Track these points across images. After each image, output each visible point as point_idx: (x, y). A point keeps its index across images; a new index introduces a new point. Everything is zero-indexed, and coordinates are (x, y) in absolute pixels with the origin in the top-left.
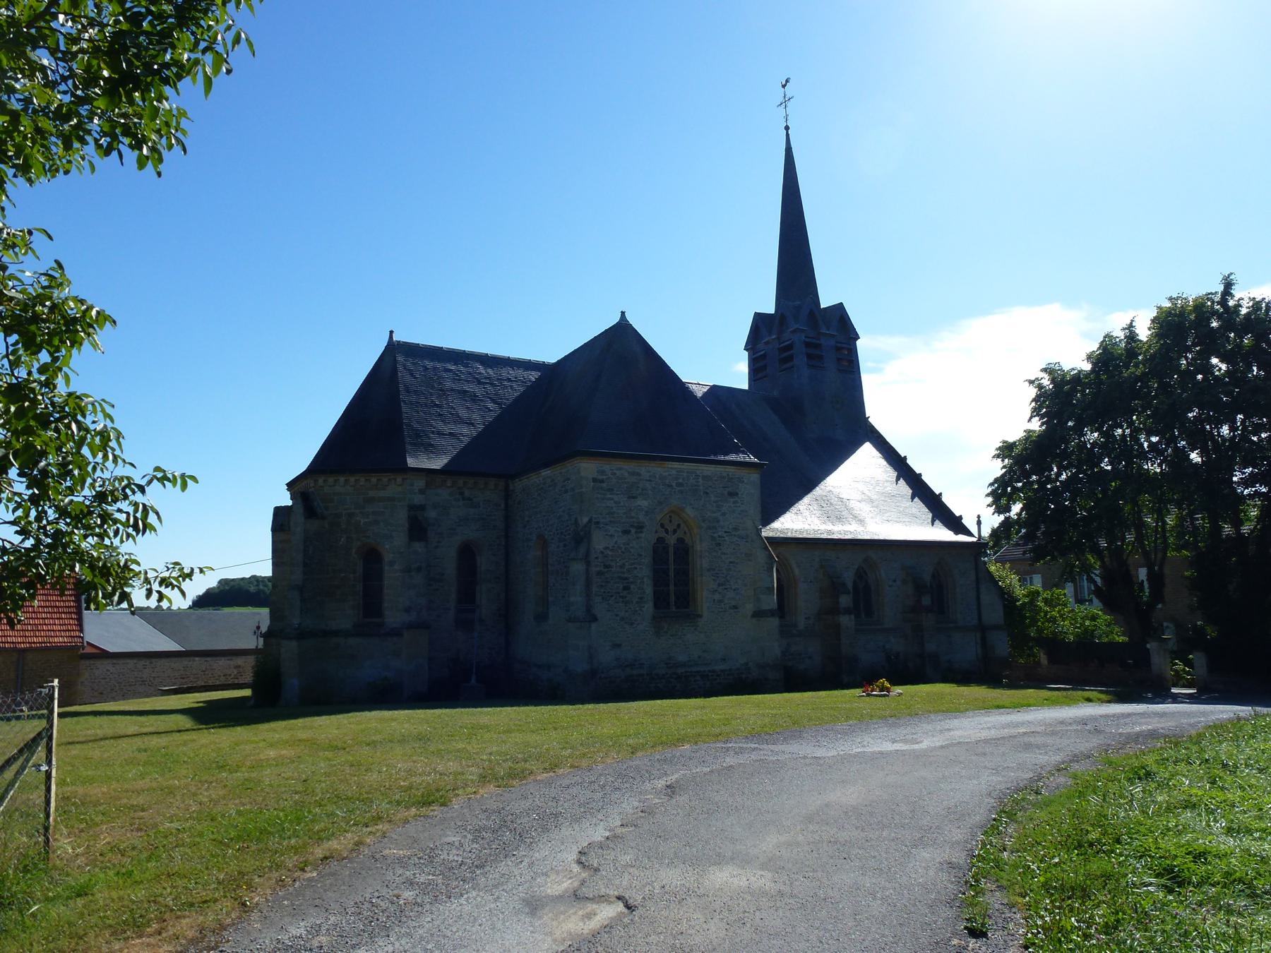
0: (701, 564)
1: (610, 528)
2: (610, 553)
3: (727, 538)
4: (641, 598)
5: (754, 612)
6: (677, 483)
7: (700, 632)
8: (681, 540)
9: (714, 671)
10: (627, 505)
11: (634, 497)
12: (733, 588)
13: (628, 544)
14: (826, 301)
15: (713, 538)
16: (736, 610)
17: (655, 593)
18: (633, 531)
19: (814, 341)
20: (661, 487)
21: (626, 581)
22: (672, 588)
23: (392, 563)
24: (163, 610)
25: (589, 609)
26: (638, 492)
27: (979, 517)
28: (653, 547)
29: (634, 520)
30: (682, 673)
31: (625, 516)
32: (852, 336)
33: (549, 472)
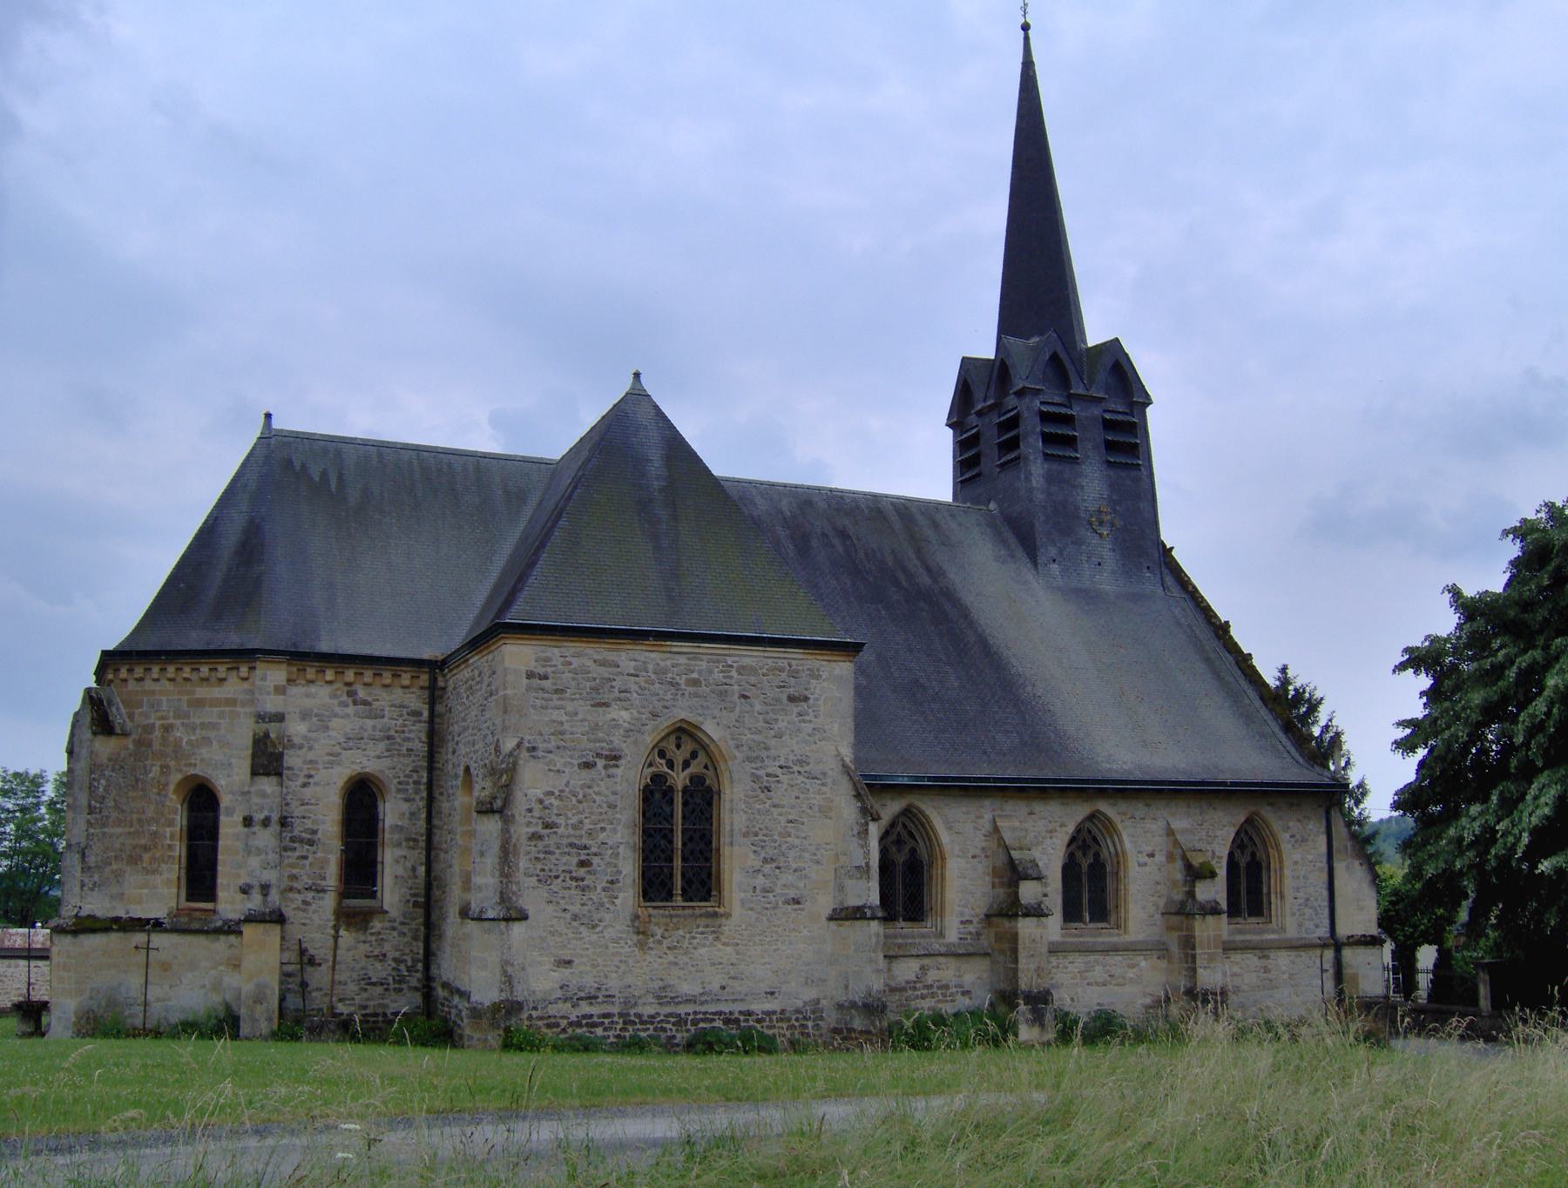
0: (732, 824)
1: (557, 759)
2: (556, 803)
4: (612, 882)
7: (724, 944)
8: (697, 780)
9: (749, 1013)
10: (589, 718)
11: (606, 705)
12: (794, 866)
13: (589, 787)
14: (1095, 334)
15: (756, 778)
16: (796, 906)
19: (1063, 411)
20: (657, 685)
22: (678, 862)
25: (504, 899)
26: (612, 696)
29: (604, 744)
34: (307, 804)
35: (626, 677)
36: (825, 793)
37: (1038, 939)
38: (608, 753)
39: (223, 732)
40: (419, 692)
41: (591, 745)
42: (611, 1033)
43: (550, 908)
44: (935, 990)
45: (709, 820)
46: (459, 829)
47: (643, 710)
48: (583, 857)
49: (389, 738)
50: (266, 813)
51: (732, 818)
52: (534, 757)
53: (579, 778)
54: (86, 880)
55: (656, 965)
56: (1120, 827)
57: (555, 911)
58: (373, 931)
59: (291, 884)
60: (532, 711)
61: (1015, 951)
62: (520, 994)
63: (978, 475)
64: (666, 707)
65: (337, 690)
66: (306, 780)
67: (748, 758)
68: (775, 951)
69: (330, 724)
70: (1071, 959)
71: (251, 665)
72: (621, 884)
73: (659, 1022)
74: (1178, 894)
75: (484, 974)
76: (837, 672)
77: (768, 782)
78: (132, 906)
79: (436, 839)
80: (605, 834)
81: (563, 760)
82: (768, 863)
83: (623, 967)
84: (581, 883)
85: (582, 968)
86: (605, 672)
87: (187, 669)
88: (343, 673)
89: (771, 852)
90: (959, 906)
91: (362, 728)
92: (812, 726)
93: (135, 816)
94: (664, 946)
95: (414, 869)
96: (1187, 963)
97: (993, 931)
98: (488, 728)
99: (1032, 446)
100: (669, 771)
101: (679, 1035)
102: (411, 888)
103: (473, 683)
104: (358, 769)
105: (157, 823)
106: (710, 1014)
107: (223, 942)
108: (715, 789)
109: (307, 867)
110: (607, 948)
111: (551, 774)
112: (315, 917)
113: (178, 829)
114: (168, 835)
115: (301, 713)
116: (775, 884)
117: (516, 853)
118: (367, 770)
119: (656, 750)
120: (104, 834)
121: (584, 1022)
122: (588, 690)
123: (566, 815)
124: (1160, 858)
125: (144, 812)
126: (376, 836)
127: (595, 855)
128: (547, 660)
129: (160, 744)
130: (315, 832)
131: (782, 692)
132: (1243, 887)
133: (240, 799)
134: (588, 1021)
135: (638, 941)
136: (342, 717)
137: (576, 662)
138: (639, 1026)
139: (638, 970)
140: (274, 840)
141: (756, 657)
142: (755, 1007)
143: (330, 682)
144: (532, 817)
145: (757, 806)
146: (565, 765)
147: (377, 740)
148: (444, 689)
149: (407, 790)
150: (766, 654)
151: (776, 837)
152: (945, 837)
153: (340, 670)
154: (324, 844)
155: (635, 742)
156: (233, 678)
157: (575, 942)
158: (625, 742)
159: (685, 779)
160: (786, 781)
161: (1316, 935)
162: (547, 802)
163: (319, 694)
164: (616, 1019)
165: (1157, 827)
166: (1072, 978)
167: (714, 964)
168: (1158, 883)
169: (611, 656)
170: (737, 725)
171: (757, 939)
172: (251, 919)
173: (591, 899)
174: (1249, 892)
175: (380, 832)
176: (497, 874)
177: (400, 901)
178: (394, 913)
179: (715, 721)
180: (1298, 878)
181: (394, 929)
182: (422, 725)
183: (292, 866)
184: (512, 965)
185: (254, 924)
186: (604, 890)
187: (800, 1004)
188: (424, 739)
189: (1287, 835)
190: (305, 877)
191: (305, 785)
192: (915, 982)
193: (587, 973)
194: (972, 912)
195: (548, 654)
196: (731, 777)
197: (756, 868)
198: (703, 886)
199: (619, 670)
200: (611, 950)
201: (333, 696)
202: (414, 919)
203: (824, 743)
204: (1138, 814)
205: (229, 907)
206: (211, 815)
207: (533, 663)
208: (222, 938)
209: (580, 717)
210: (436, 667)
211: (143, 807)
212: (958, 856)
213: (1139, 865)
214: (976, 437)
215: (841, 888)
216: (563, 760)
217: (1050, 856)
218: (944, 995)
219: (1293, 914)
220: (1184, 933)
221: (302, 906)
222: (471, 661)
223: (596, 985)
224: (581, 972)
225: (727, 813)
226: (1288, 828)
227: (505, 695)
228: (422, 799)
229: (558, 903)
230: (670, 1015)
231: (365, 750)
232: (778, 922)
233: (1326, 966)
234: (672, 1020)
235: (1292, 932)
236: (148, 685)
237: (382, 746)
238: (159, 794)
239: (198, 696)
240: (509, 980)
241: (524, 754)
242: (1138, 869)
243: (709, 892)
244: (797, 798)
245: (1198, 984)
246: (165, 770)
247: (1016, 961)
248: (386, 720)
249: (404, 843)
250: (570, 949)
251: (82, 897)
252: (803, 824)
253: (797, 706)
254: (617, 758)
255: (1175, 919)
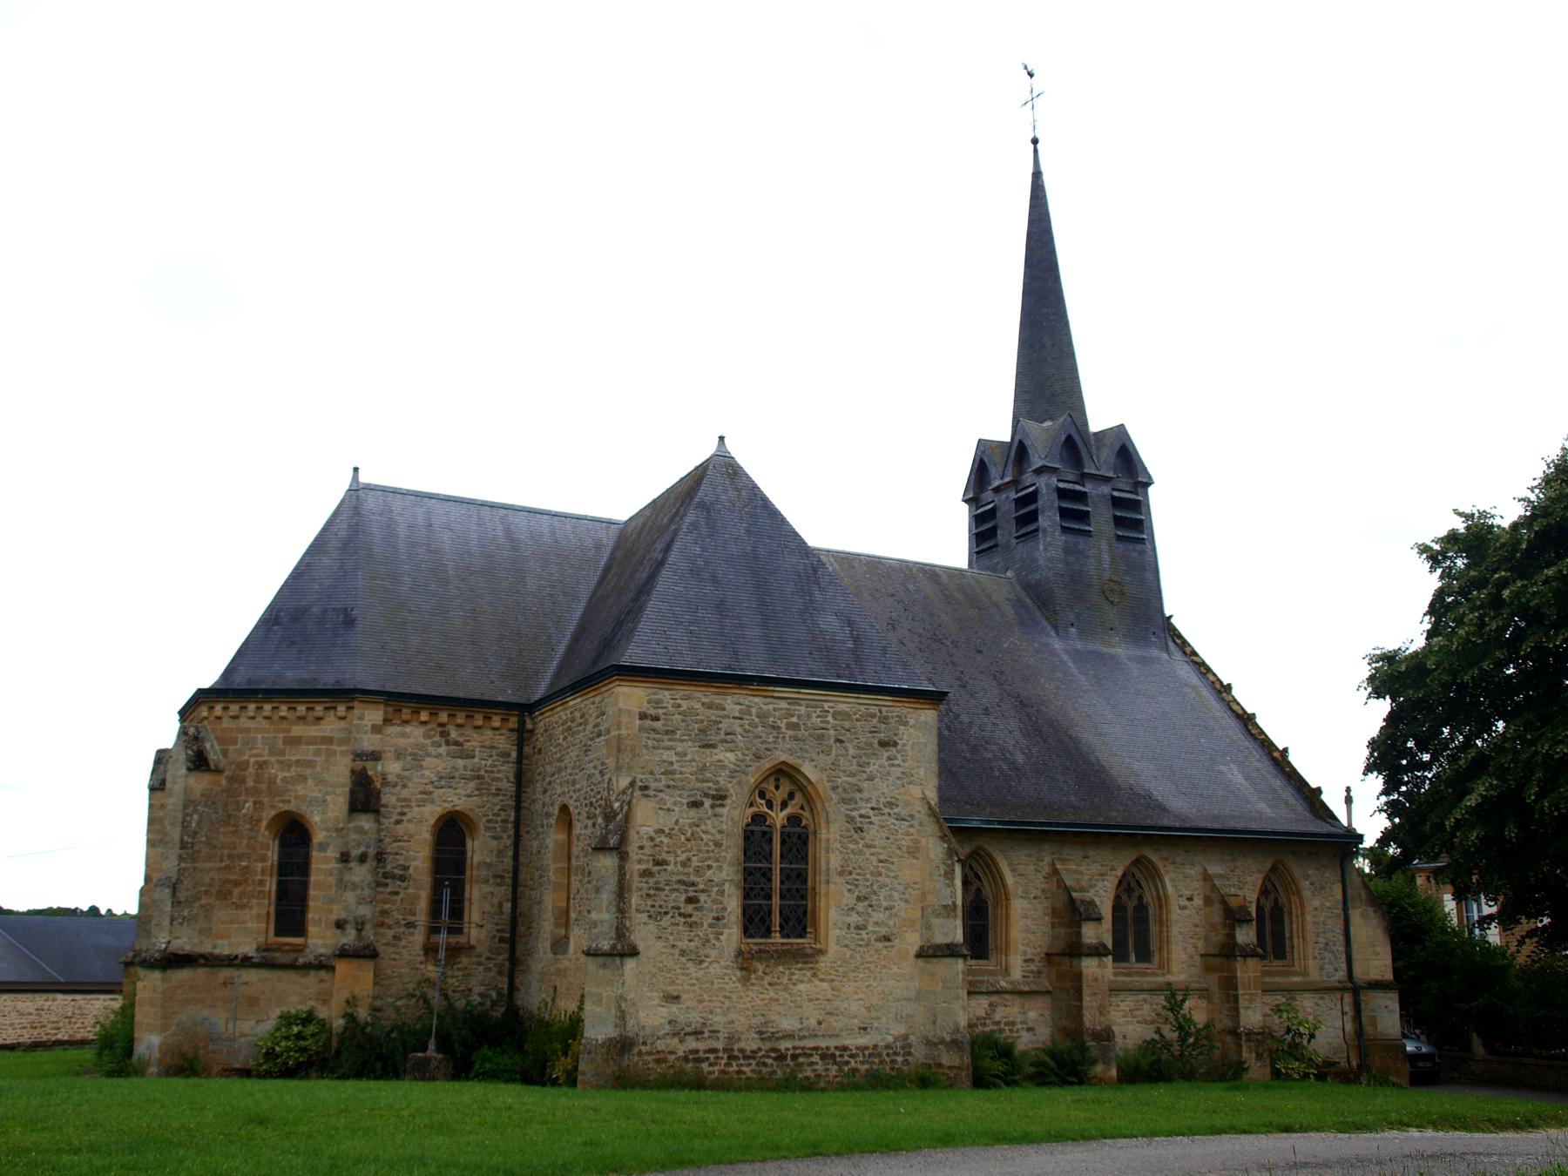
0: (828, 863)
2: (666, 840)
3: (873, 819)
4: (718, 919)
5: (922, 947)
6: (787, 724)
7: (822, 980)
8: (794, 820)
9: (845, 1048)
10: (697, 759)
11: (713, 746)
13: (698, 826)
15: (850, 820)
16: (887, 944)
18: (708, 803)
19: (1078, 488)
20: (760, 729)
22: (776, 901)
23: (323, 847)
24: (101, 916)
25: (621, 932)
26: (718, 738)
27: (1348, 790)
29: (711, 784)
30: (787, 1049)
31: (693, 777)
34: (400, 841)
35: (732, 720)
37: (1100, 977)
39: (318, 769)
40: (508, 734)
41: (699, 785)
42: (716, 1068)
43: (659, 944)
44: (1002, 1026)
45: (805, 859)
46: (552, 867)
47: (747, 752)
48: (691, 894)
49: (479, 777)
50: (363, 849)
51: (828, 857)
52: (647, 796)
55: (758, 1002)
58: (459, 966)
60: (644, 751)
61: (1078, 991)
63: (996, 546)
64: (767, 749)
65: (430, 730)
66: (399, 817)
67: (843, 799)
68: (867, 987)
69: (423, 763)
70: (1122, 997)
71: (349, 705)
72: (726, 921)
73: (761, 1057)
74: (1216, 935)
75: (599, 1009)
76: (922, 718)
77: (861, 822)
79: (522, 876)
80: (711, 871)
81: (672, 800)
82: (863, 901)
83: (727, 1003)
84: (688, 919)
85: (688, 1004)
86: (713, 714)
87: (284, 708)
90: (1023, 945)
91: (453, 767)
93: (226, 852)
95: (501, 905)
96: (1228, 1002)
99: (1049, 519)
102: (497, 924)
104: (448, 806)
106: (809, 1049)
107: (312, 979)
110: (712, 983)
112: (404, 952)
113: (269, 864)
114: (259, 870)
116: (867, 921)
117: (630, 890)
118: (458, 808)
120: (195, 869)
121: (691, 1057)
122: (696, 731)
123: (675, 852)
124: (1198, 901)
125: (234, 848)
126: (463, 873)
127: (702, 891)
128: (658, 702)
130: (406, 868)
132: (1268, 930)
133: (334, 835)
134: (694, 1057)
135: (742, 977)
137: (685, 705)
138: (742, 1061)
139: (741, 1006)
141: (849, 703)
143: (424, 723)
145: (852, 846)
146: (675, 803)
147: (468, 779)
148: (532, 731)
149: (495, 828)
151: (868, 876)
154: (415, 880)
155: (740, 783)
156: (331, 717)
158: (730, 782)
160: (877, 823)
161: (1336, 978)
162: (658, 840)
163: (413, 735)
164: (721, 1055)
166: (1124, 1017)
167: (812, 1000)
168: (1197, 926)
169: (718, 700)
170: (833, 767)
171: (851, 975)
172: (344, 953)
173: (698, 935)
179: (814, 763)
180: (1318, 923)
181: (480, 964)
182: (510, 765)
184: (625, 1000)
185: (348, 959)
186: (710, 926)
187: (890, 1039)
188: (512, 779)
189: (1308, 883)
191: (398, 822)
192: (985, 1018)
193: (693, 1009)
196: (827, 817)
197: (850, 906)
198: (799, 923)
199: (725, 713)
201: (427, 736)
204: (1178, 860)
205: (320, 942)
208: (312, 973)
209: (689, 757)
213: (1180, 908)
216: (672, 800)
217: (1103, 896)
220: (1225, 974)
222: (571, 703)
223: (702, 1020)
225: (823, 852)
226: (1309, 875)
227: (619, 735)
228: (509, 836)
230: (773, 1050)
231: (456, 789)
232: (871, 959)
234: (773, 1055)
235: (1314, 975)
236: (244, 722)
237: (472, 785)
238: (251, 830)
240: (622, 1016)
241: (638, 793)
242: (1179, 911)
243: (804, 928)
244: (888, 838)
246: (258, 805)
247: (1080, 999)
248: (476, 760)
249: (492, 881)
253: (887, 751)
254: (723, 798)
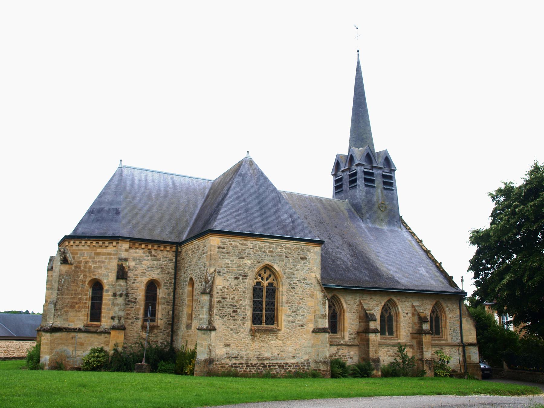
0: (282, 299)
1: (227, 276)
2: (226, 291)
4: (244, 318)
7: (279, 340)
8: (271, 284)
9: (287, 364)
10: (238, 262)
11: (243, 258)
12: (302, 314)
13: (237, 286)
15: (290, 284)
16: (302, 328)
17: (253, 315)
18: (241, 278)
20: (259, 252)
21: (235, 307)
22: (264, 312)
23: (107, 291)
25: (210, 322)
27: (462, 277)
28: (254, 288)
29: (242, 271)
30: (267, 364)
32: (392, 168)
33: (197, 242)
34: (134, 289)
35: (250, 249)
36: (311, 290)
37: (375, 340)
38: (243, 274)
39: (106, 264)
40: (172, 253)
41: (238, 272)
43: (223, 326)
44: (342, 357)
45: (274, 298)
46: (187, 299)
47: (255, 260)
48: (235, 309)
49: (162, 268)
50: (121, 292)
52: (220, 275)
53: (234, 282)
54: (56, 314)
55: (257, 347)
56: (398, 304)
57: (225, 327)
58: (154, 333)
59: (127, 316)
60: (219, 259)
62: (213, 355)
64: (262, 260)
66: (134, 281)
69: (143, 262)
70: (383, 347)
72: (246, 319)
75: (202, 349)
76: (316, 250)
77: (294, 285)
78: (71, 323)
79: (176, 302)
81: (229, 276)
83: (247, 347)
84: (234, 318)
86: (243, 247)
87: (94, 243)
88: (148, 246)
89: (294, 309)
92: (308, 267)
93: (73, 292)
94: (260, 340)
95: (168, 312)
96: (420, 350)
97: (360, 337)
98: (202, 265)
99: (361, 182)
100: (262, 281)
101: (264, 371)
102: (167, 319)
103: (195, 250)
104: (151, 278)
105: (82, 295)
106: (275, 363)
108: (277, 287)
109: (133, 311)
110: (241, 340)
111: (225, 281)
112: (135, 328)
113: (88, 297)
114: (85, 299)
115: (133, 258)
117: (213, 307)
118: (154, 278)
119: (258, 274)
120: (62, 298)
121: (234, 366)
122: (237, 253)
123: (229, 295)
124: (410, 315)
127: (238, 308)
128: (224, 243)
129: (84, 268)
130: (136, 299)
131: (299, 256)
132: (434, 325)
133: (111, 287)
134: (235, 366)
136: (147, 260)
137: (234, 244)
138: (251, 368)
140: (123, 301)
142: (288, 361)
144: (218, 295)
145: (290, 294)
146: (230, 278)
147: (158, 268)
149: (167, 285)
150: (294, 243)
151: (296, 304)
152: (345, 306)
153: (146, 244)
155: (252, 271)
157: (231, 338)
159: (267, 284)
160: (299, 286)
161: (457, 342)
162: (223, 290)
163: (139, 253)
164: (244, 365)
165: (409, 304)
168: (409, 323)
169: (245, 242)
171: (290, 338)
172: (114, 328)
173: (237, 324)
174: (435, 326)
175: (158, 299)
176: (208, 314)
177: (164, 323)
178: (162, 327)
181: (161, 332)
182: (173, 264)
183: (128, 310)
184: (211, 346)
185: (115, 330)
186: (241, 320)
188: (173, 268)
190: (132, 314)
191: (134, 283)
192: (335, 354)
194: (353, 331)
195: (225, 241)
196: (282, 284)
197: (290, 314)
199: (247, 247)
200: (243, 341)
201: (144, 253)
202: (168, 329)
203: (311, 273)
204: (403, 300)
205: (105, 324)
206: (100, 292)
207: (220, 243)
208: (103, 335)
209: (235, 262)
210: (179, 244)
211: (76, 289)
212: (349, 312)
214: (341, 179)
215: (316, 322)
216: (229, 276)
217: (377, 312)
218: (345, 358)
219: (450, 335)
220: (419, 340)
221: (131, 324)
223: (238, 353)
224: (233, 349)
225: (280, 295)
226: (448, 306)
229: (226, 325)
231: (154, 271)
233: (460, 352)
234: (262, 365)
235: (449, 341)
236: (80, 247)
237: (159, 270)
238: (82, 285)
239: (97, 252)
240: (210, 351)
241: (217, 274)
242: (403, 318)
243: (274, 322)
244: (303, 291)
245: (424, 357)
246: (85, 276)
247: (368, 348)
248: (161, 262)
249: (166, 304)
250: (229, 340)
251: (54, 320)
252: (304, 300)
254: (246, 276)
255: (416, 335)
